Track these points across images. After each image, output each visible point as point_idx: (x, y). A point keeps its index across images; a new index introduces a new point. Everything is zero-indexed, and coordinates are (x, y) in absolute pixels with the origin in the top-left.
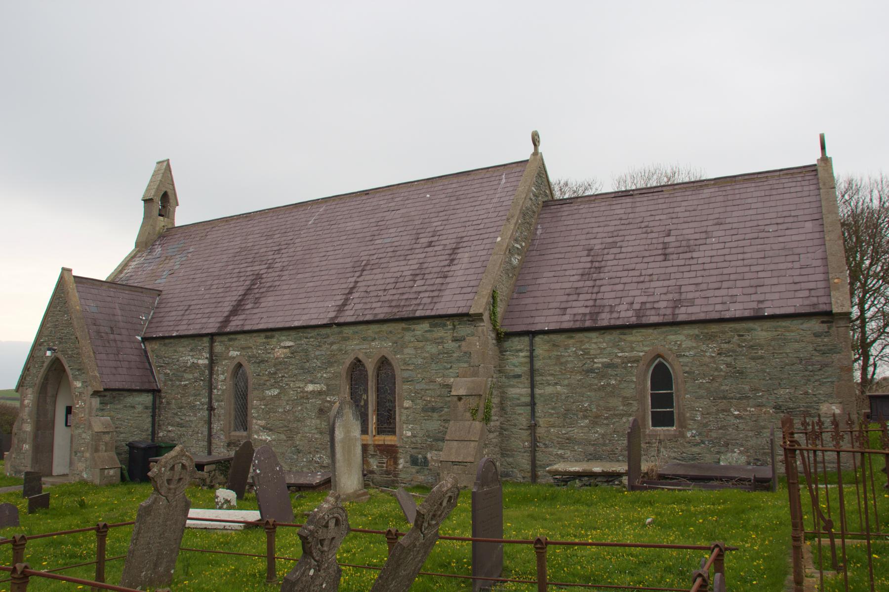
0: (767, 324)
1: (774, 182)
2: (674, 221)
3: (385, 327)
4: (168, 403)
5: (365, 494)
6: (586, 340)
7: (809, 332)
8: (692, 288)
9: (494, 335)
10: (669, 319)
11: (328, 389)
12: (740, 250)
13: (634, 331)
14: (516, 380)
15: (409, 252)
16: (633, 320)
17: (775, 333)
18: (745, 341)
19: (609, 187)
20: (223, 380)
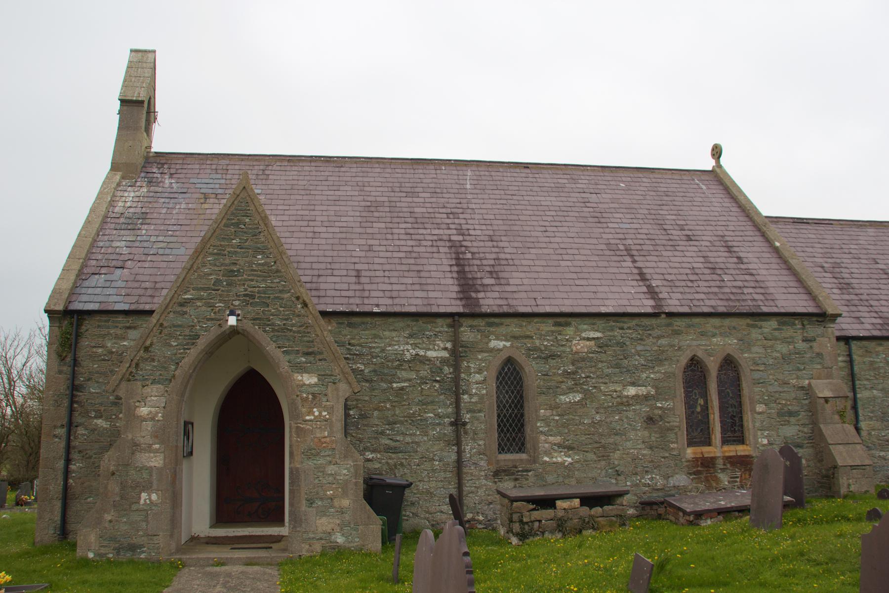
20: (480, 383)
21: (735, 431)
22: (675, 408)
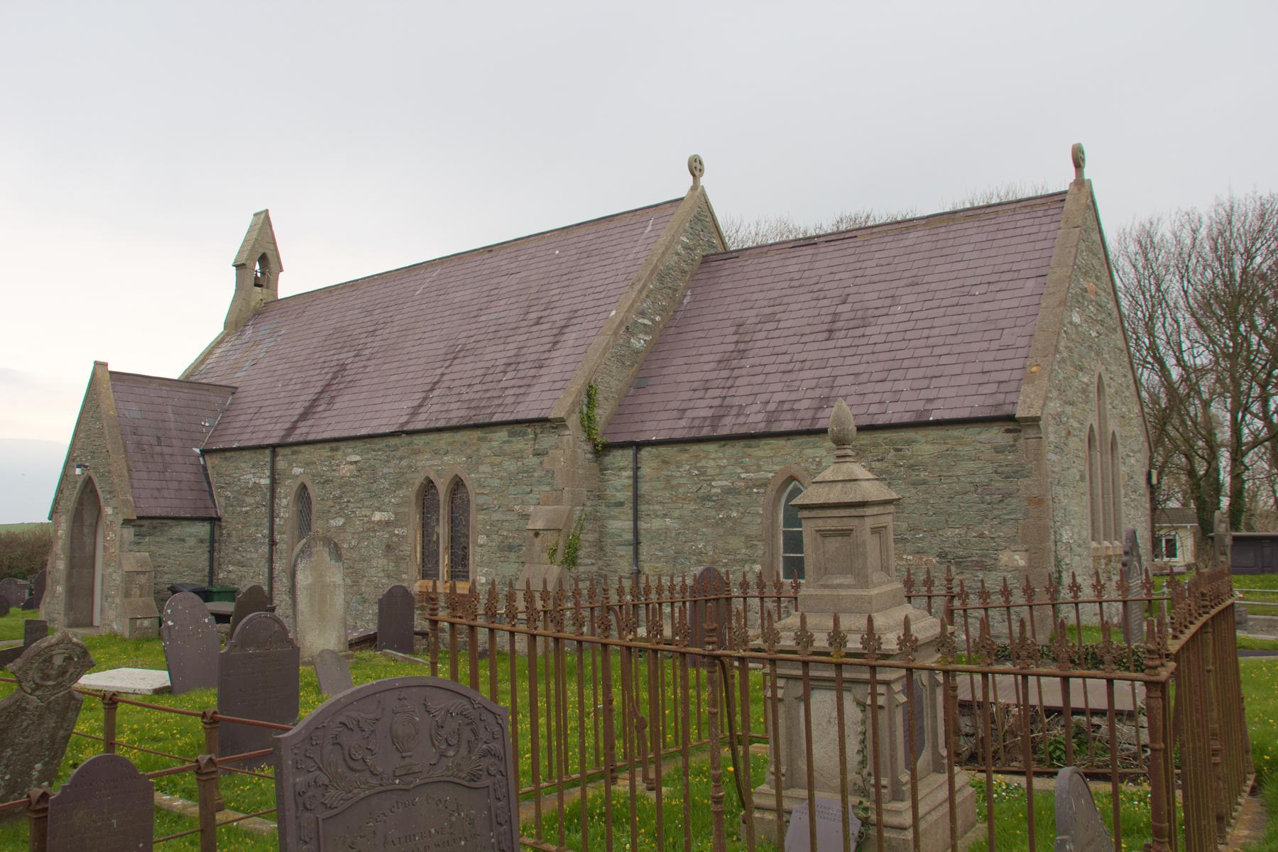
0: (934, 433)
1: (1006, 219)
2: (858, 281)
3: (459, 436)
4: (229, 535)
5: (348, 657)
6: (702, 455)
7: (989, 446)
8: (850, 379)
9: (589, 448)
10: (805, 426)
11: (397, 520)
12: (928, 323)
13: (763, 442)
14: (618, 510)
15: (511, 333)
16: (761, 427)
17: (944, 447)
18: (903, 457)
19: (828, 227)
20: (286, 503)
21: (460, 567)
22: (410, 533)
